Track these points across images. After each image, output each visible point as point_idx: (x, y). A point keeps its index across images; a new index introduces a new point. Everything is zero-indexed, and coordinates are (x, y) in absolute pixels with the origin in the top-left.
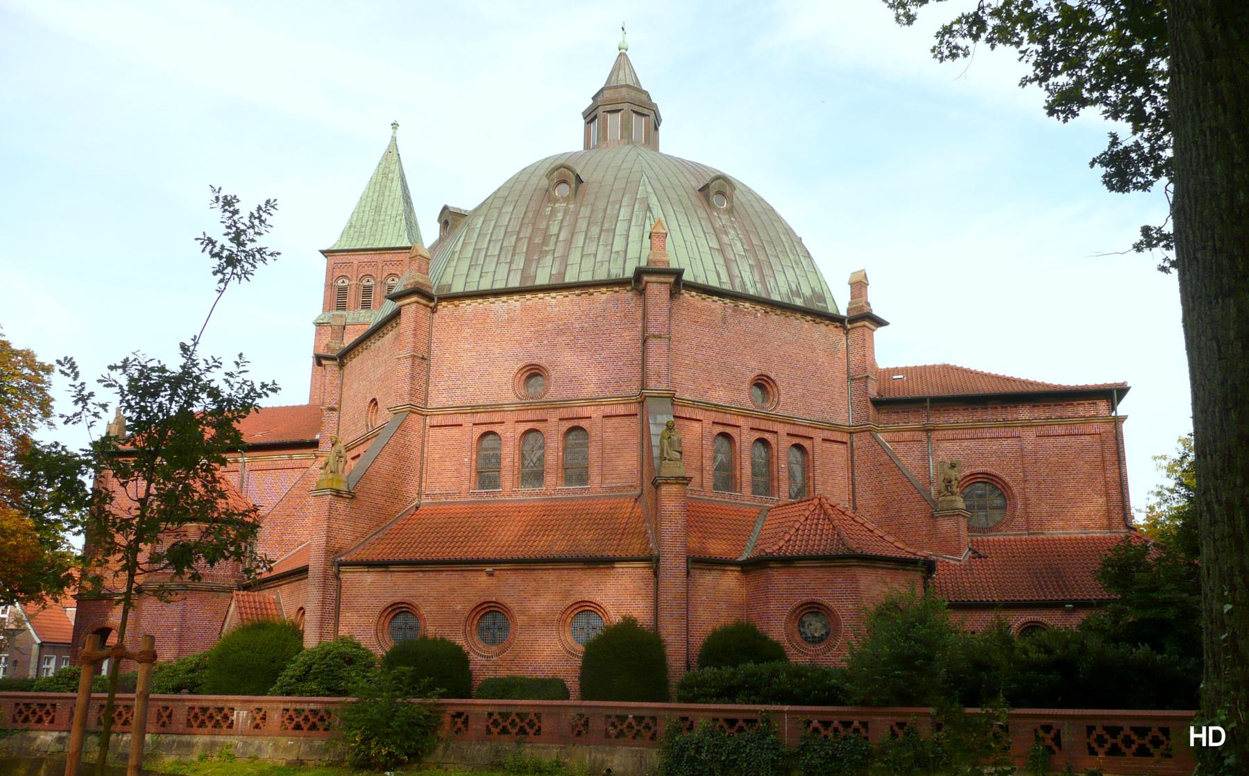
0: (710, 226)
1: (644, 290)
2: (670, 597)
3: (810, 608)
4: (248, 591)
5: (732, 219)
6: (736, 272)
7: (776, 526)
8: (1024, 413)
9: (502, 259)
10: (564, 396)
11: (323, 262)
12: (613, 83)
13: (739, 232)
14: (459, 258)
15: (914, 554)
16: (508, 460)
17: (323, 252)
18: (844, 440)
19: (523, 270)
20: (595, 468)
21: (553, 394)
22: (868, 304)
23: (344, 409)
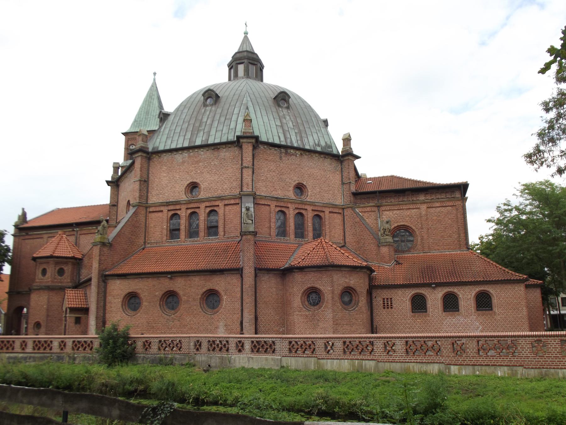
0: (277, 115)
1: (242, 146)
2: (247, 286)
3: (312, 290)
4: (77, 289)
5: (289, 111)
6: (289, 136)
7: (302, 252)
8: (422, 197)
9: (181, 134)
10: (207, 196)
11: (124, 137)
12: (241, 50)
13: (291, 117)
14: (162, 135)
15: (361, 264)
16: (183, 226)
17: (123, 134)
18: (340, 212)
19: (190, 139)
20: (221, 228)
21: (203, 195)
22: (351, 149)
23: (119, 205)
